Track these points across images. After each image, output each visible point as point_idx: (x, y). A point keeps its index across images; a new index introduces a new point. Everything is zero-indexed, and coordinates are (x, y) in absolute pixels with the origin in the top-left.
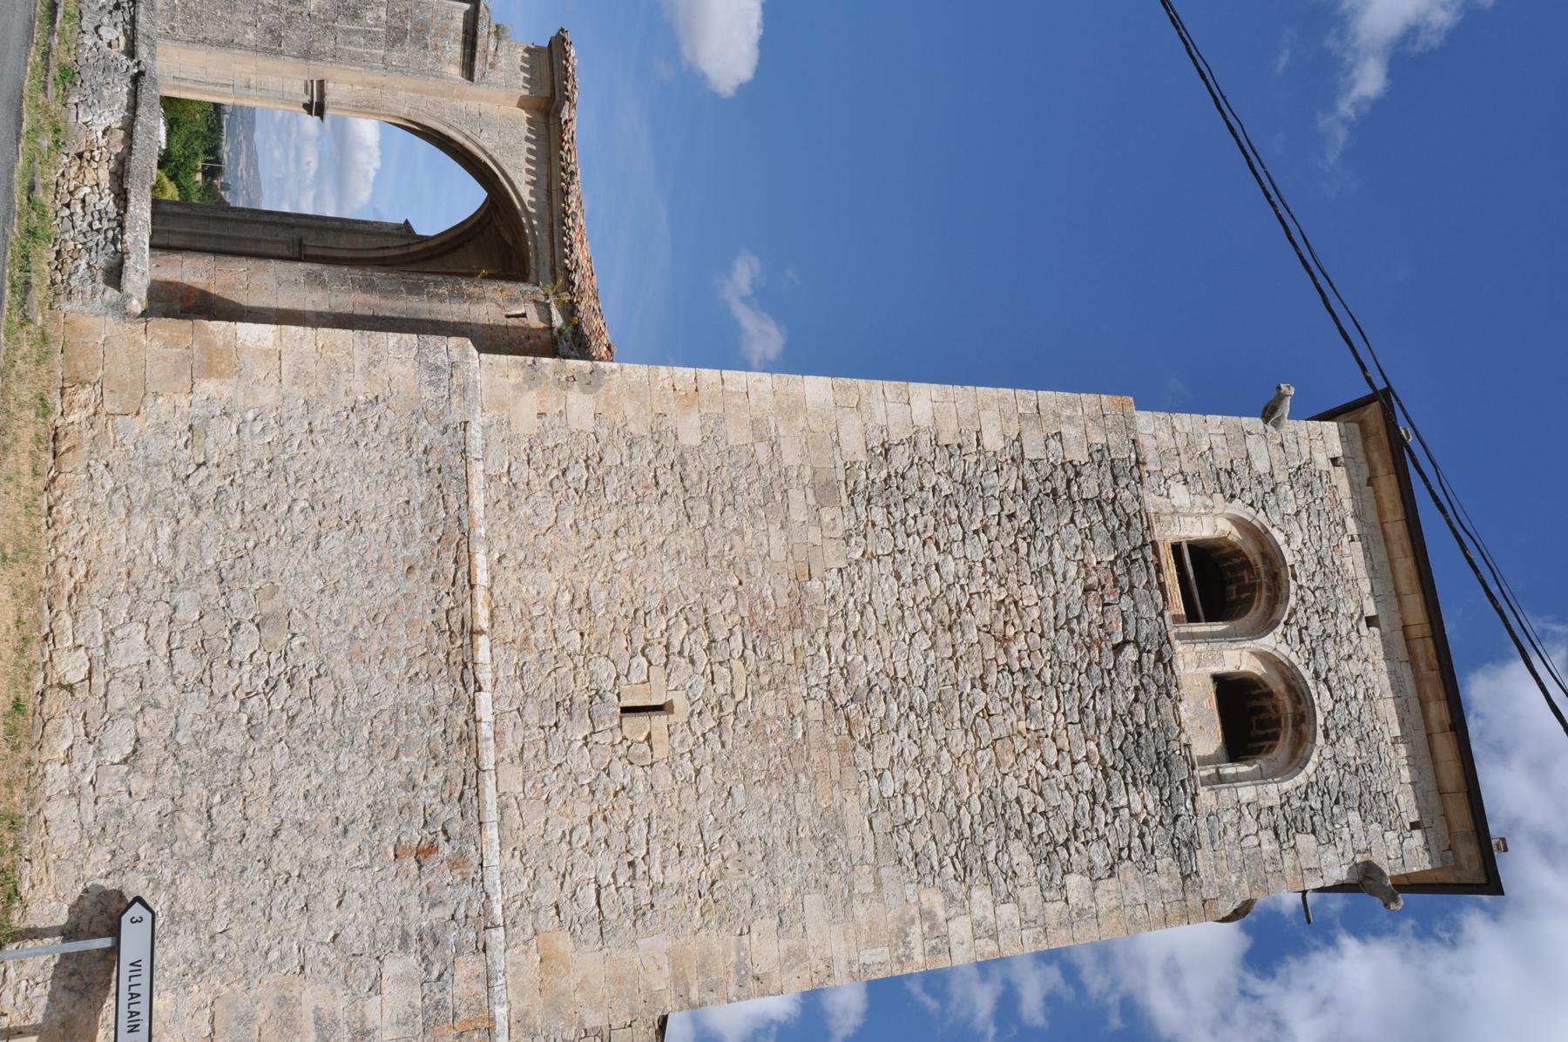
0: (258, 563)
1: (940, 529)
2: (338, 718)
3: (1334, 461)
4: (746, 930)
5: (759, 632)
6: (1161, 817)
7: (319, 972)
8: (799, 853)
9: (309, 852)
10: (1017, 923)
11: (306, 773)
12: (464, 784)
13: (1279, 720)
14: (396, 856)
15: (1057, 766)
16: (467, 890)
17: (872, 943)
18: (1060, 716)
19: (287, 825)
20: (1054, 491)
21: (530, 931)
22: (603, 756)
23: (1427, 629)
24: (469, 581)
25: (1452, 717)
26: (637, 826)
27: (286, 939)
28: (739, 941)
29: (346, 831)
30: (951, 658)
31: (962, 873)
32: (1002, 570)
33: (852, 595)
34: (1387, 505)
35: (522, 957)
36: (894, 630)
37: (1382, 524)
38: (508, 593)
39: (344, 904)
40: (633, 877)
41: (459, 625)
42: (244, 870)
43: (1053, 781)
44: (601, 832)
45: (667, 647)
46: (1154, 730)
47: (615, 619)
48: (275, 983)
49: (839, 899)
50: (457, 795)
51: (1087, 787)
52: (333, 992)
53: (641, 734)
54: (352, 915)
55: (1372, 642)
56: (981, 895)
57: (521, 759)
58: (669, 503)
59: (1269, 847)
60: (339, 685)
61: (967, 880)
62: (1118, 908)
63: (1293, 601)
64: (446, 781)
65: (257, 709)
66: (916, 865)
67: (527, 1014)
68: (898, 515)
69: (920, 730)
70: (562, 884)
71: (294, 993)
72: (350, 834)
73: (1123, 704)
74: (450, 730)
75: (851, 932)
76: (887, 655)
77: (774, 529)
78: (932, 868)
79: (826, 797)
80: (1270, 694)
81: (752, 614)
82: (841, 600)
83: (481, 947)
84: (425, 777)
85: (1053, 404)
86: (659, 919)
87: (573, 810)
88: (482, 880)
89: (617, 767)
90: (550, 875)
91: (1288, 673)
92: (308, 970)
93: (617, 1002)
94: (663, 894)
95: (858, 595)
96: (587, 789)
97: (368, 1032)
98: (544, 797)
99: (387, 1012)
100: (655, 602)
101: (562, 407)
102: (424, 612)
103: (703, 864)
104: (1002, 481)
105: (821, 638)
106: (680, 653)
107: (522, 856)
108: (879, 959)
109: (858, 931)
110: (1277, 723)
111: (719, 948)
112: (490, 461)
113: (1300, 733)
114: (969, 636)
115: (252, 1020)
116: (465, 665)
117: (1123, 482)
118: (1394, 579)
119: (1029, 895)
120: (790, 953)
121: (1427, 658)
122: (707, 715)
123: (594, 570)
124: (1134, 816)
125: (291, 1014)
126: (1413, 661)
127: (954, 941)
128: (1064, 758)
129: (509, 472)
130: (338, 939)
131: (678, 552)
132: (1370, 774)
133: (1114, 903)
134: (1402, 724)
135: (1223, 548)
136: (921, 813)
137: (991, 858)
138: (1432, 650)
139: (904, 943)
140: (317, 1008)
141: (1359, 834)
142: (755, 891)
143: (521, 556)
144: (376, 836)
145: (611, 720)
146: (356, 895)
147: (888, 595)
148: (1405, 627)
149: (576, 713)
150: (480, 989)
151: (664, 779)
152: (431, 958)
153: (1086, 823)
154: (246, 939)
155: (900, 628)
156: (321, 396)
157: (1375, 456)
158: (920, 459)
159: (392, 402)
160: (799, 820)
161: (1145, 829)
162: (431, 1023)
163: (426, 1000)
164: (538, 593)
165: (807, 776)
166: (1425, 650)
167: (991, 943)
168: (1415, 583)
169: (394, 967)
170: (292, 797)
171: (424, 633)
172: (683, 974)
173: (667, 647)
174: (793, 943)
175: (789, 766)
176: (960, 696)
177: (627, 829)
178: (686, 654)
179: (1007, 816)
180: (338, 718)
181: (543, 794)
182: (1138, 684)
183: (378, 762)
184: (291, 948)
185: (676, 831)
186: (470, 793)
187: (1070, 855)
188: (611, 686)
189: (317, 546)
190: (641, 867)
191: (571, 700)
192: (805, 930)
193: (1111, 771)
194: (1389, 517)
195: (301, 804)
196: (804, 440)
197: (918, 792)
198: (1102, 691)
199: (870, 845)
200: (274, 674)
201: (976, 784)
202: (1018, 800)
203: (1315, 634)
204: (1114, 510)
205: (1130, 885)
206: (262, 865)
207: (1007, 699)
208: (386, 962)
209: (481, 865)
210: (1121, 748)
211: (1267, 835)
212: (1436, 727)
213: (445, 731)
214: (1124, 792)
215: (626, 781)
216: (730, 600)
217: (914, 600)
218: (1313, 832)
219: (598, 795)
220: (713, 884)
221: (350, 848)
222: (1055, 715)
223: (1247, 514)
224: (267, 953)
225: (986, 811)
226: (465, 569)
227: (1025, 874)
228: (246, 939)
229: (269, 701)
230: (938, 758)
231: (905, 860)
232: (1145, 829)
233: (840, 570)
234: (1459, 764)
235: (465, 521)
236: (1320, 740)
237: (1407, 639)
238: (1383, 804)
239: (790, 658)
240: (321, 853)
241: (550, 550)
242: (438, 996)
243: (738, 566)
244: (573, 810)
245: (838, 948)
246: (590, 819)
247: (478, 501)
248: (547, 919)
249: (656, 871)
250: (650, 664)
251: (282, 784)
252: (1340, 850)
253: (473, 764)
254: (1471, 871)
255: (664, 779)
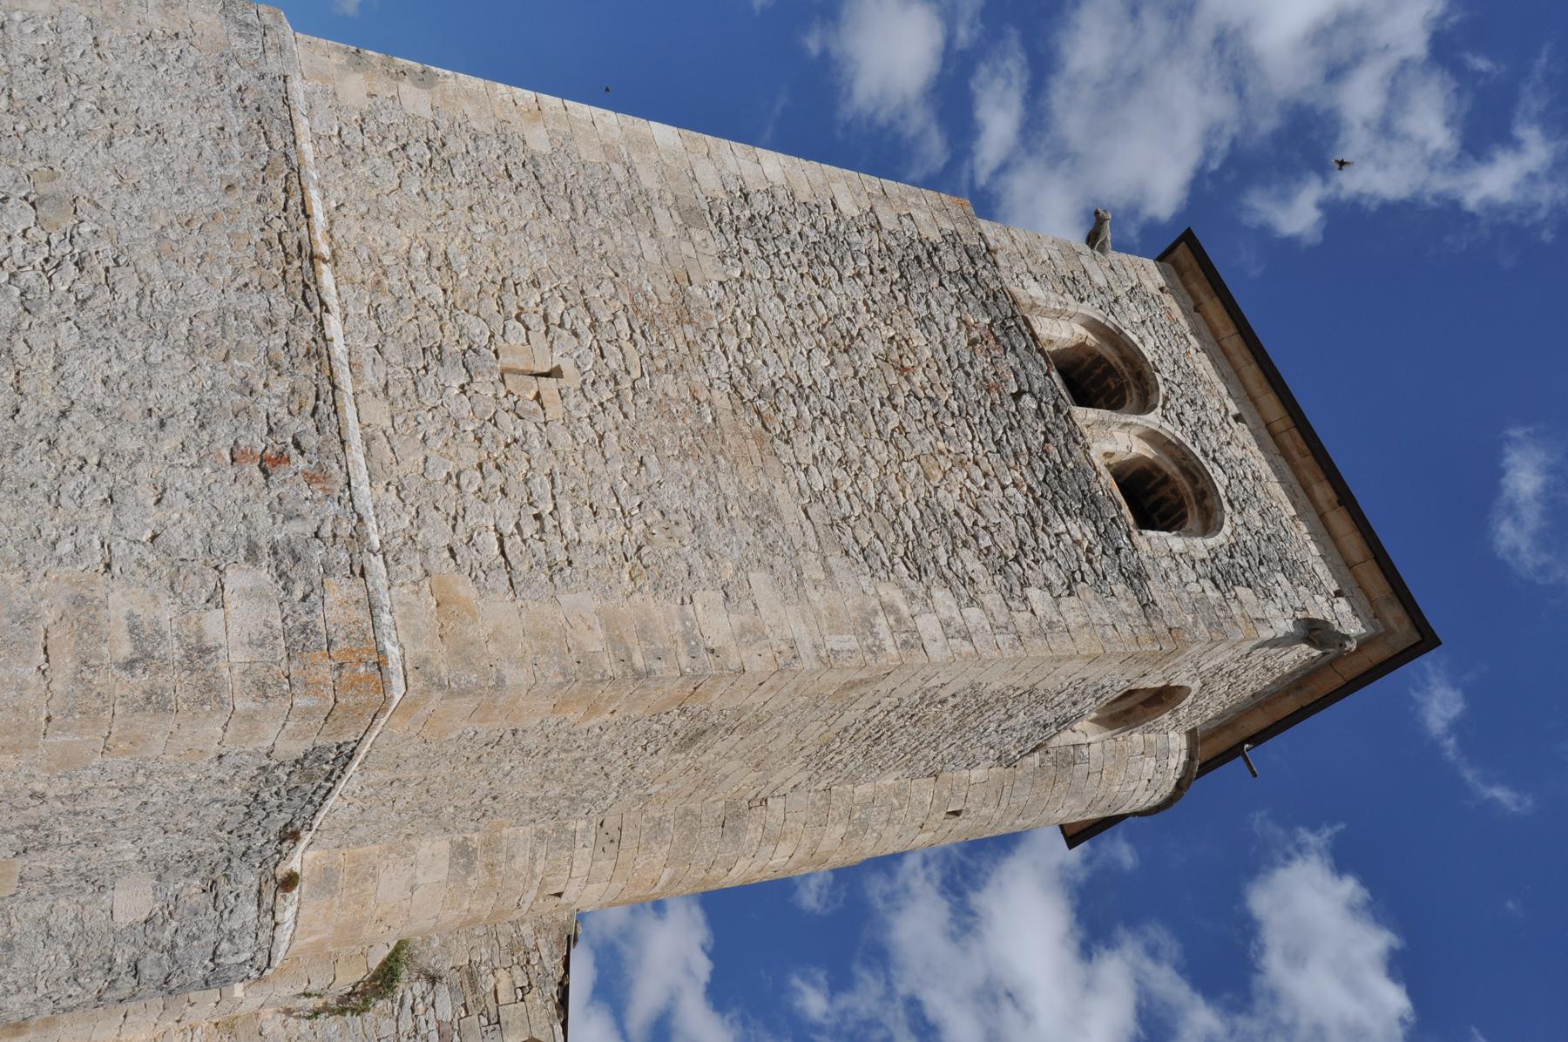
0: (31, 145)
1: (815, 267)
2: (144, 309)
3: (1161, 289)
4: (687, 600)
5: (644, 324)
6: (1103, 547)
7: (133, 574)
8: (733, 531)
9: (113, 439)
10: (988, 627)
11: (105, 357)
12: (317, 398)
13: (1182, 500)
14: (233, 460)
15: (986, 487)
16: (332, 508)
17: (837, 629)
18: (976, 444)
19: (79, 407)
20: (917, 258)
21: (419, 571)
22: (487, 406)
23: (1288, 421)
24: (304, 211)
25: (1337, 493)
26: (538, 480)
27: (82, 531)
28: (682, 610)
29: (162, 424)
30: (854, 377)
31: (916, 573)
32: (885, 310)
33: (738, 306)
34: (1218, 324)
35: (414, 597)
36: (788, 342)
37: (1218, 342)
38: (351, 236)
39: (164, 502)
40: (542, 530)
41: (295, 247)
42: (18, 447)
43: (987, 499)
44: (496, 479)
45: (545, 318)
46: (1072, 470)
47: (480, 283)
48: (68, 579)
49: (788, 582)
50: (309, 409)
51: (1022, 510)
52: (154, 598)
53: (528, 390)
54: (176, 516)
55: (1243, 433)
56: (941, 595)
57: (387, 394)
58: (525, 195)
59: (1213, 595)
60: (144, 279)
61: (924, 579)
62: (1087, 625)
63: (1163, 390)
64: (293, 392)
65: (33, 283)
66: (865, 559)
67: (426, 661)
68: (770, 248)
69: (839, 436)
70: (454, 527)
71: (97, 593)
72: (169, 428)
73: (1036, 443)
74: (293, 344)
75: (810, 615)
76: (788, 364)
77: (644, 236)
78: (883, 564)
79: (752, 481)
80: (1166, 479)
81: (635, 304)
82: (729, 308)
83: (357, 571)
84: (266, 385)
85: (898, 191)
86: (580, 577)
87: (457, 453)
88: (351, 500)
89: (505, 419)
90: (438, 516)
91: (1178, 455)
92: (116, 569)
93: (542, 659)
94: (581, 551)
95: (745, 306)
96: (471, 437)
97: (208, 650)
98: (420, 436)
99: (234, 630)
100: (525, 275)
101: (394, 93)
102: (250, 229)
103: (623, 528)
104: (866, 241)
105: (713, 337)
106: (561, 325)
107: (398, 492)
108: (847, 646)
109: (817, 616)
110: (1181, 504)
111: (659, 614)
112: (316, 120)
113: (1206, 509)
114: (866, 360)
115: (34, 618)
116: (306, 286)
117: (980, 264)
118: (1245, 387)
119: (992, 600)
120: (743, 631)
121: (1297, 446)
122: (601, 386)
123: (450, 235)
124: (1077, 543)
125: (93, 617)
126: (1284, 452)
127: (926, 638)
128: (992, 481)
129: (339, 134)
130: (158, 540)
131: (543, 237)
132: (1281, 543)
133: (1081, 619)
134: (1294, 504)
135: (1082, 361)
136: (858, 511)
137: (943, 562)
138: (1299, 438)
139: (871, 633)
140: (131, 616)
141: (1291, 594)
142: (690, 561)
143: (363, 209)
144: (205, 436)
145: (491, 374)
146: (181, 494)
147: (775, 311)
148: (1268, 425)
149: (448, 361)
150: (361, 617)
151: (563, 440)
152: (292, 575)
153: (1031, 542)
154: (23, 523)
155: (794, 342)
156: (106, 16)
157: (1195, 286)
158: (780, 208)
159: (195, 40)
160: (725, 498)
161: (1091, 556)
162: (299, 648)
163: (289, 621)
164: (388, 244)
165: (725, 458)
166: (1293, 440)
167: (966, 643)
168: (1265, 384)
169: (238, 579)
170: (85, 379)
171: (252, 247)
172: (621, 637)
173: (545, 318)
174: (746, 619)
175: (703, 446)
176: (872, 410)
177: (526, 482)
178: (568, 326)
179: (949, 525)
180: (144, 309)
181: (417, 432)
182: (1044, 429)
183: (203, 360)
184: (90, 542)
185: (586, 489)
186: (325, 409)
187: (1024, 570)
188: (485, 342)
189: (109, 144)
190: (549, 523)
191: (439, 347)
192: (756, 607)
193: (1042, 500)
194: (1223, 334)
195: (99, 388)
196: (659, 171)
197: (850, 491)
198: (1011, 429)
199: (810, 533)
200: (58, 253)
201: (909, 491)
202: (957, 513)
203: (1192, 421)
204: (978, 283)
205: (1093, 606)
206: (44, 445)
207: (920, 421)
208: (229, 572)
209: (349, 484)
210: (1044, 480)
211: (1207, 584)
212: (1325, 507)
213: (287, 344)
214: (1059, 519)
215: (518, 434)
216: (607, 288)
217: (803, 321)
218: (1249, 586)
219: (486, 443)
220: (639, 548)
221: (169, 444)
222: (972, 442)
223: (1099, 316)
224: (54, 544)
225: (925, 518)
226: (298, 199)
227: (983, 581)
228: (23, 523)
229: (50, 279)
230: (863, 463)
231: (851, 552)
232: (1091, 556)
233: (721, 283)
234: (1358, 534)
235: (293, 157)
236: (1227, 508)
237: (1274, 436)
238: (1303, 570)
239: (684, 349)
240: (129, 444)
241: (395, 210)
242: (305, 619)
243: (611, 261)
244: (457, 453)
245: (796, 628)
246: (480, 466)
247: (307, 147)
248: (440, 562)
249: (568, 526)
250: (528, 329)
251: (71, 364)
252: (1280, 606)
253: (326, 382)
254: (1404, 633)
255: (563, 440)
